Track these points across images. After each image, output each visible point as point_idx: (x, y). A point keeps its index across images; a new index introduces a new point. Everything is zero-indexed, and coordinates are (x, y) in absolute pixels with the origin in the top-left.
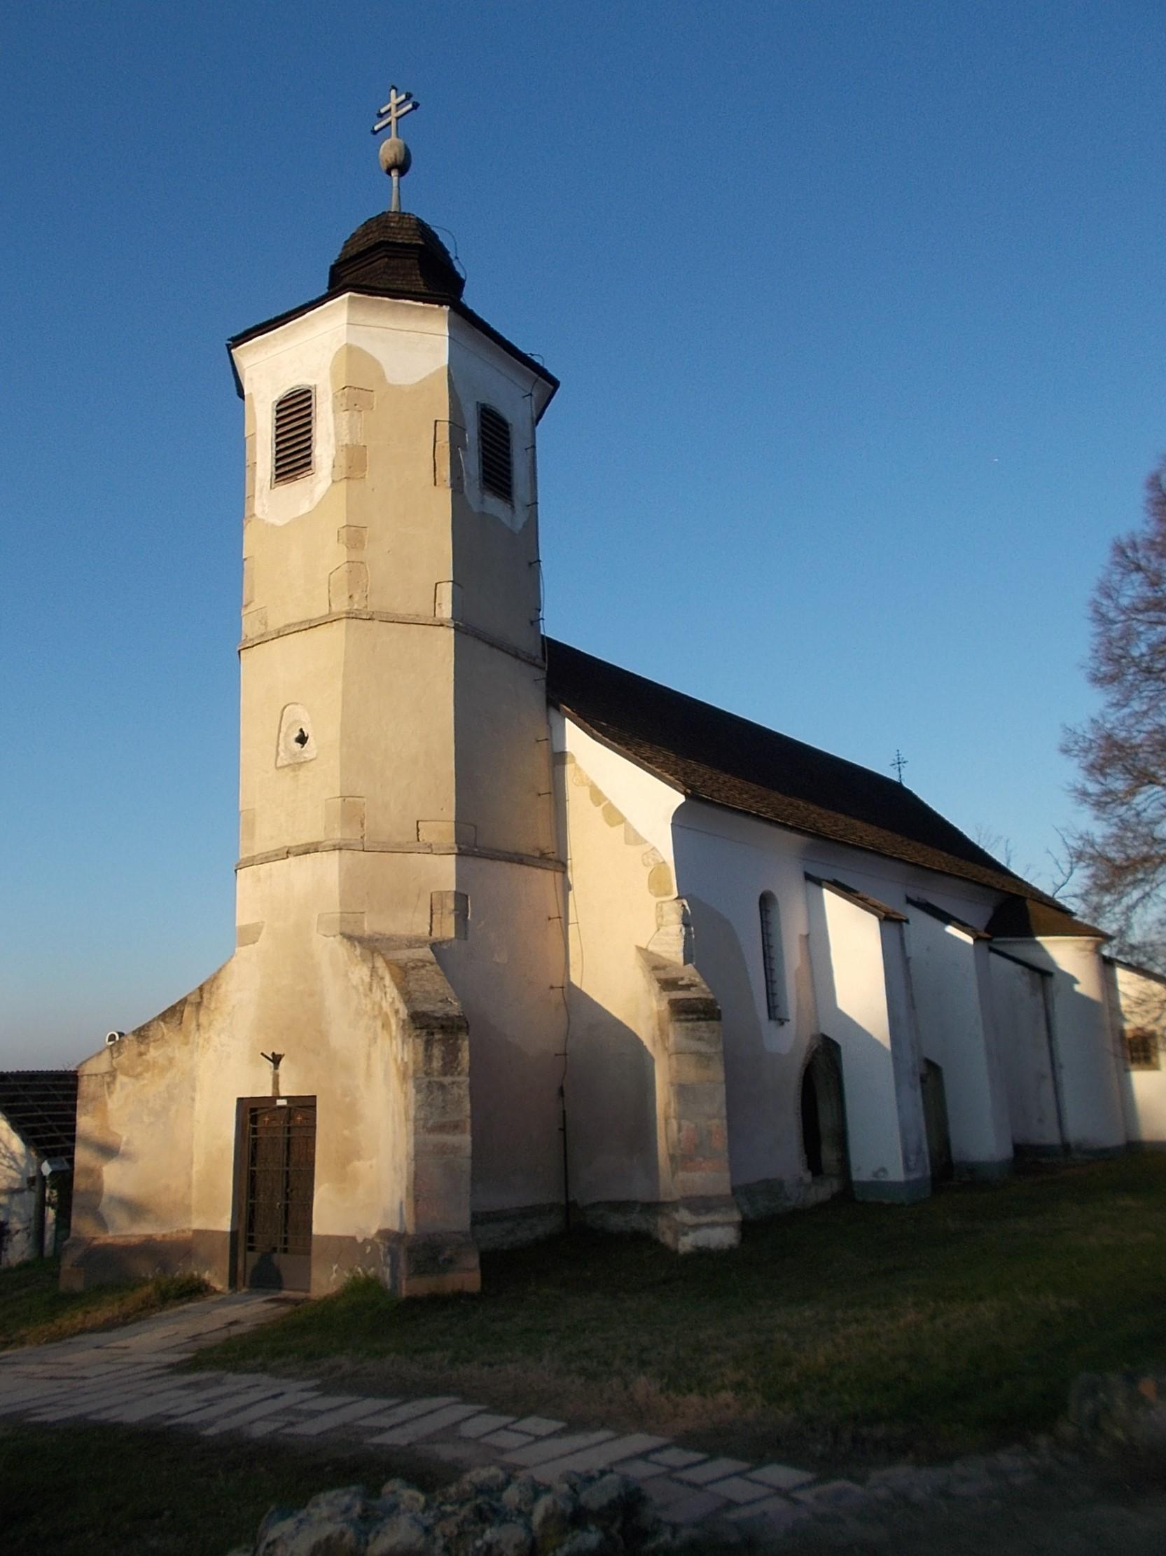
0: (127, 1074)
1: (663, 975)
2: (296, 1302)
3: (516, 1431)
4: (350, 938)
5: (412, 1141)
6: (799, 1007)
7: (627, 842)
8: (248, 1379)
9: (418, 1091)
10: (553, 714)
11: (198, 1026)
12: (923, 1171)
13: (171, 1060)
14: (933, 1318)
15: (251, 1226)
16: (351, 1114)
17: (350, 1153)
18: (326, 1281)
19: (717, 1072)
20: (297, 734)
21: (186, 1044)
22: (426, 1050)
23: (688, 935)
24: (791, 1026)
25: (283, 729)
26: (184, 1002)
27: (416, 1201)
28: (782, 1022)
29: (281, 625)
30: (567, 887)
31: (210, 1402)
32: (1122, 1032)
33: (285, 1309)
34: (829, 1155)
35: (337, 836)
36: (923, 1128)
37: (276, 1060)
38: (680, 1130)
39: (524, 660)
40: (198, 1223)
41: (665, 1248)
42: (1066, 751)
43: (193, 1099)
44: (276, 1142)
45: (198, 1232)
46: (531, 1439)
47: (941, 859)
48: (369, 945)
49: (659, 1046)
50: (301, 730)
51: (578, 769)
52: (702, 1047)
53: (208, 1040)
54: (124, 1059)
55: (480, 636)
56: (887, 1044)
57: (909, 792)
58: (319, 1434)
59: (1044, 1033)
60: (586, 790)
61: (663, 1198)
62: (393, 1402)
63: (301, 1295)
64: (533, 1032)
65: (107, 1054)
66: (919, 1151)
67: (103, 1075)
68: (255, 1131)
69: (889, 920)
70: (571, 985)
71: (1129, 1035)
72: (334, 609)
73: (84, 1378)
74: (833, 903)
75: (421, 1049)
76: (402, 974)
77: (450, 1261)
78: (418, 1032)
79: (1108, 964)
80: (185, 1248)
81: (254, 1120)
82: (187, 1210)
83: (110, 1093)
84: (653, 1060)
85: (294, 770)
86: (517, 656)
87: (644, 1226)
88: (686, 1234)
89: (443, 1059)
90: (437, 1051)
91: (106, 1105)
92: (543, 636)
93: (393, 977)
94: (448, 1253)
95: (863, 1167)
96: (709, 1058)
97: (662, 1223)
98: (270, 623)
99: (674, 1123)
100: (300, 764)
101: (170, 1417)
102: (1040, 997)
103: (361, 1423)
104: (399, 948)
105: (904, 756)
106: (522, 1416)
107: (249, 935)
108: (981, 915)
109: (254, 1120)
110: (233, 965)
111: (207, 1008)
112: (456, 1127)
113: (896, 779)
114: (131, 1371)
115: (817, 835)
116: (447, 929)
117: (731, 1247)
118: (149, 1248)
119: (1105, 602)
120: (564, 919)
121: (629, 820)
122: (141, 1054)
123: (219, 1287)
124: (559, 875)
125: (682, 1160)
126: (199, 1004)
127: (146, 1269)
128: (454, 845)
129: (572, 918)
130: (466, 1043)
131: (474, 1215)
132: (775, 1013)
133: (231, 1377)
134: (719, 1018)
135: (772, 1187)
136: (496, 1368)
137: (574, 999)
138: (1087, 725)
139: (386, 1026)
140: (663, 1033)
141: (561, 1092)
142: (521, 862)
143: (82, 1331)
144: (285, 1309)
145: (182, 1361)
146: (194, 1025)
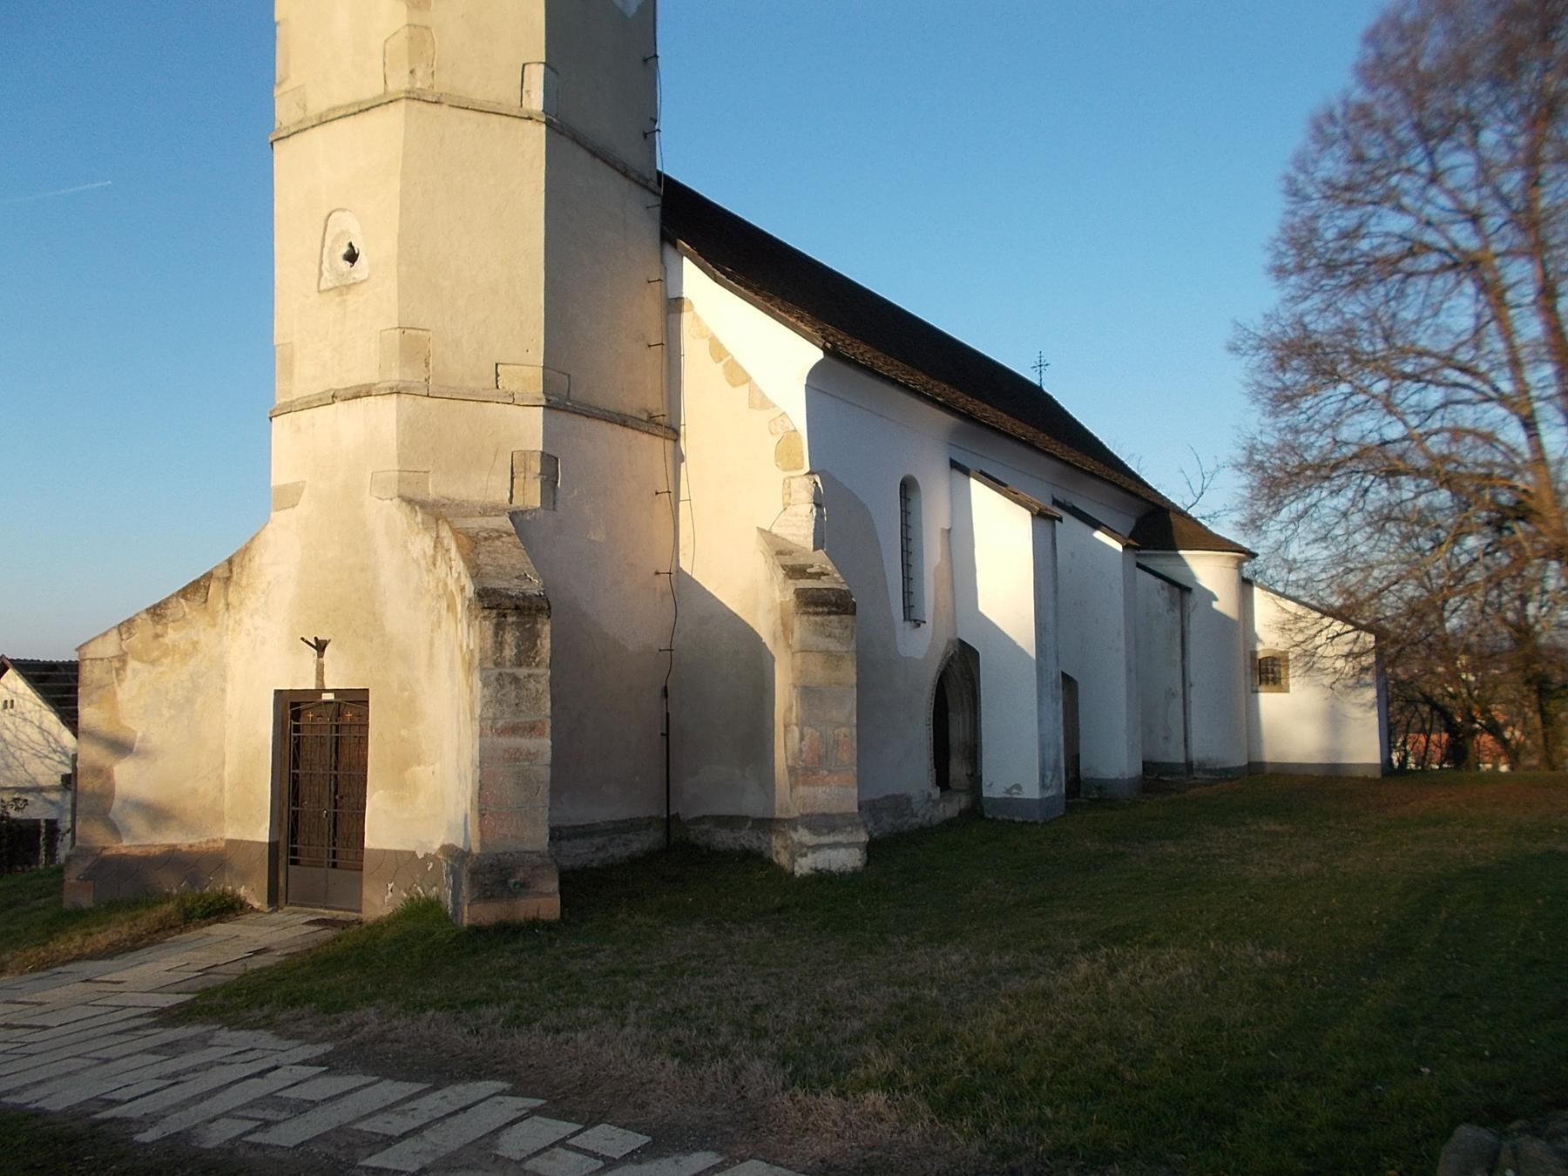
0: (141, 660)
1: (789, 561)
2: (345, 924)
3: (577, 1150)
4: (410, 502)
5: (477, 746)
6: (936, 608)
7: (752, 405)
8: (243, 1037)
9: (485, 685)
10: (669, 251)
11: (228, 605)
12: (1058, 788)
13: (195, 644)
14: (1112, 970)
15: (294, 835)
16: (410, 711)
17: (407, 758)
18: (380, 901)
19: (849, 673)
20: (345, 249)
21: (214, 626)
22: (496, 634)
23: (819, 517)
24: (927, 628)
25: (328, 243)
26: (209, 576)
27: (482, 815)
28: (918, 623)
29: (323, 108)
30: (679, 458)
31: (175, 1079)
32: (1254, 653)
33: (329, 933)
34: (958, 770)
35: (395, 377)
36: (1062, 742)
37: (320, 646)
38: (802, 739)
39: (632, 179)
40: (231, 833)
41: (780, 868)
42: (1234, 349)
43: (223, 690)
44: (321, 744)
45: (230, 842)
46: (601, 1164)
47: (1090, 465)
48: (434, 512)
49: (781, 643)
50: (350, 245)
51: (696, 318)
52: (833, 646)
53: (239, 622)
54: (135, 641)
55: (578, 140)
56: (1032, 653)
57: (1050, 397)
58: (297, 1147)
59: (1178, 649)
60: (706, 343)
61: (778, 815)
62: (418, 1087)
63: (353, 915)
64: (633, 623)
65: (114, 635)
66: (1057, 766)
67: (110, 660)
68: (297, 729)
69: (1040, 516)
70: (679, 570)
71: (1260, 656)
72: (390, 87)
73: (45, 1028)
74: (980, 493)
75: (490, 633)
76: (472, 545)
77: (523, 885)
78: (486, 612)
79: (1246, 583)
80: (218, 860)
81: (296, 715)
82: (220, 817)
83: (120, 681)
84: (773, 658)
85: (341, 294)
86: (625, 174)
87: (756, 844)
88: (805, 855)
89: (518, 646)
90: (510, 637)
91: (115, 694)
92: (659, 174)
93: (459, 547)
94: (520, 876)
95: (995, 785)
96: (840, 658)
97: (777, 843)
98: (310, 106)
99: (796, 731)
100: (348, 287)
101: (113, 1103)
102: (1178, 613)
103: (364, 1126)
104: (471, 515)
105: (1046, 358)
106: (589, 1124)
107: (289, 497)
108: (1127, 524)
109: (296, 715)
110: (269, 533)
111: (238, 584)
112: (532, 729)
113: (1037, 383)
114: (105, 1020)
115: (968, 417)
116: (531, 496)
117: (855, 870)
118: (173, 859)
119: (1302, 177)
120: (674, 494)
121: (756, 378)
122: (157, 636)
123: (257, 905)
124: (669, 444)
125: (803, 772)
126: (228, 579)
127: (172, 884)
128: (542, 396)
129: (683, 495)
130: (547, 628)
131: (552, 830)
132: (911, 614)
133: (225, 1035)
134: (854, 613)
135: (899, 803)
136: (562, 1037)
137: (681, 587)
138: (1259, 320)
139: (451, 608)
140: (786, 627)
141: (665, 689)
142: (624, 424)
143: (78, 958)
144: (329, 933)
145: (179, 1005)
146: (221, 605)
